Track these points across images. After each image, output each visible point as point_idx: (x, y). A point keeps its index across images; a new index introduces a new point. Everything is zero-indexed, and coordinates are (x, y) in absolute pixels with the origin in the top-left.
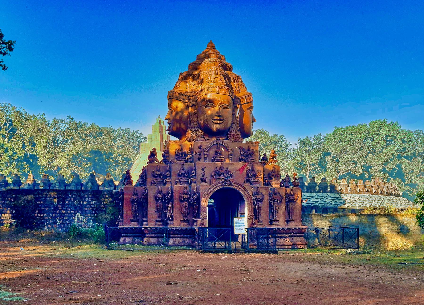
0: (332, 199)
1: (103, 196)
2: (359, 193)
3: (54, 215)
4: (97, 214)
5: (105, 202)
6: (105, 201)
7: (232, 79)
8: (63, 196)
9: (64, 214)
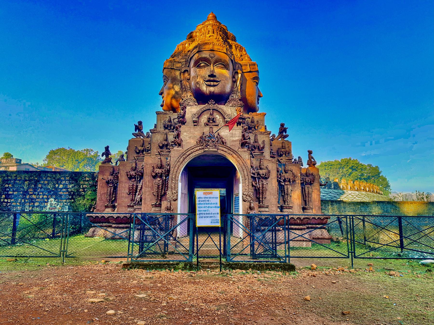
0: (337, 194)
1: (83, 179)
2: (357, 190)
3: (23, 201)
4: (74, 199)
5: (84, 186)
6: (84, 184)
7: (234, 47)
8: (36, 179)
9: (35, 199)
